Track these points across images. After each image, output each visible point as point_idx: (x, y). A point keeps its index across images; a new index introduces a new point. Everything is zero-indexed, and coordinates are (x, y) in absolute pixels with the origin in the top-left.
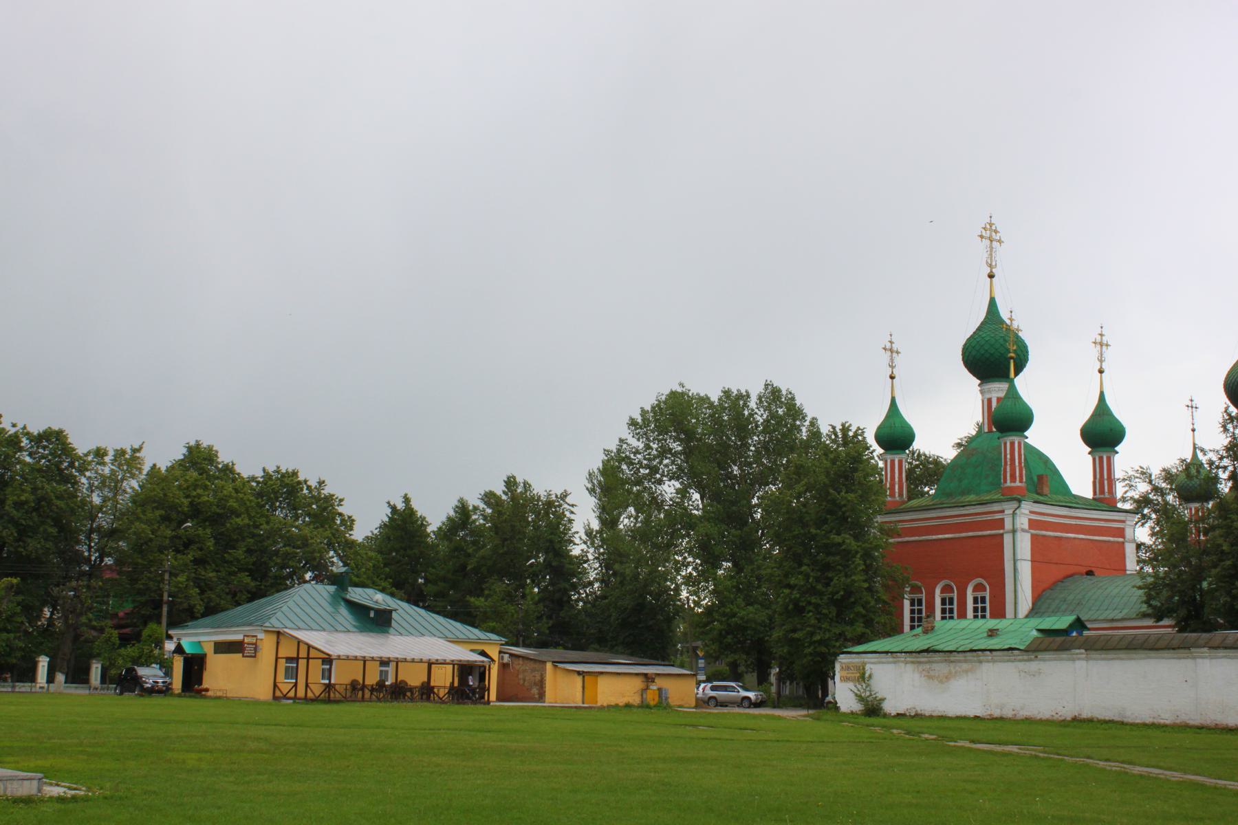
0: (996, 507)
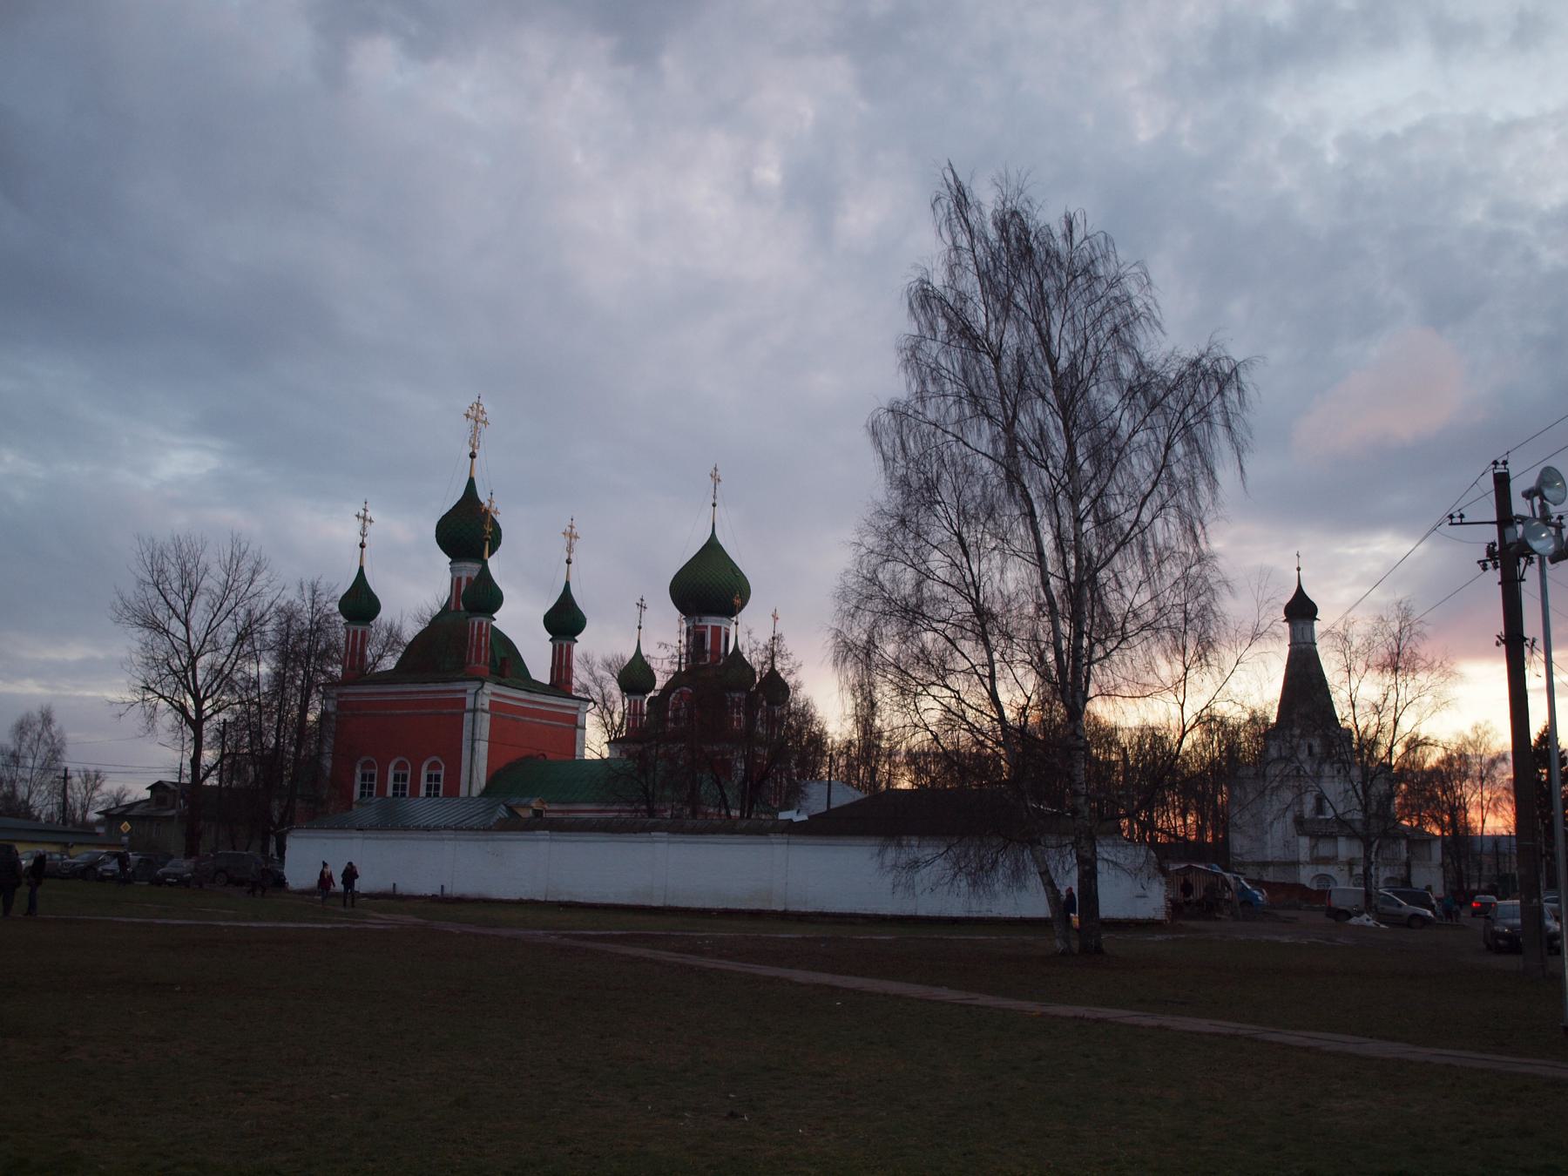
0: (458, 686)
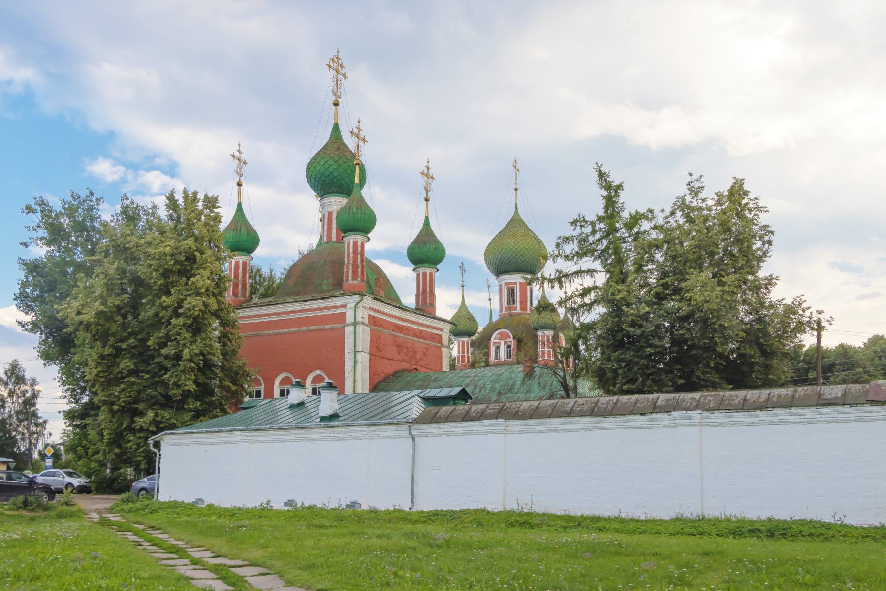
0: (338, 302)
